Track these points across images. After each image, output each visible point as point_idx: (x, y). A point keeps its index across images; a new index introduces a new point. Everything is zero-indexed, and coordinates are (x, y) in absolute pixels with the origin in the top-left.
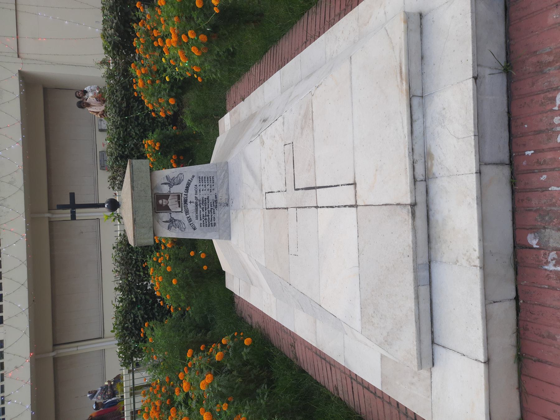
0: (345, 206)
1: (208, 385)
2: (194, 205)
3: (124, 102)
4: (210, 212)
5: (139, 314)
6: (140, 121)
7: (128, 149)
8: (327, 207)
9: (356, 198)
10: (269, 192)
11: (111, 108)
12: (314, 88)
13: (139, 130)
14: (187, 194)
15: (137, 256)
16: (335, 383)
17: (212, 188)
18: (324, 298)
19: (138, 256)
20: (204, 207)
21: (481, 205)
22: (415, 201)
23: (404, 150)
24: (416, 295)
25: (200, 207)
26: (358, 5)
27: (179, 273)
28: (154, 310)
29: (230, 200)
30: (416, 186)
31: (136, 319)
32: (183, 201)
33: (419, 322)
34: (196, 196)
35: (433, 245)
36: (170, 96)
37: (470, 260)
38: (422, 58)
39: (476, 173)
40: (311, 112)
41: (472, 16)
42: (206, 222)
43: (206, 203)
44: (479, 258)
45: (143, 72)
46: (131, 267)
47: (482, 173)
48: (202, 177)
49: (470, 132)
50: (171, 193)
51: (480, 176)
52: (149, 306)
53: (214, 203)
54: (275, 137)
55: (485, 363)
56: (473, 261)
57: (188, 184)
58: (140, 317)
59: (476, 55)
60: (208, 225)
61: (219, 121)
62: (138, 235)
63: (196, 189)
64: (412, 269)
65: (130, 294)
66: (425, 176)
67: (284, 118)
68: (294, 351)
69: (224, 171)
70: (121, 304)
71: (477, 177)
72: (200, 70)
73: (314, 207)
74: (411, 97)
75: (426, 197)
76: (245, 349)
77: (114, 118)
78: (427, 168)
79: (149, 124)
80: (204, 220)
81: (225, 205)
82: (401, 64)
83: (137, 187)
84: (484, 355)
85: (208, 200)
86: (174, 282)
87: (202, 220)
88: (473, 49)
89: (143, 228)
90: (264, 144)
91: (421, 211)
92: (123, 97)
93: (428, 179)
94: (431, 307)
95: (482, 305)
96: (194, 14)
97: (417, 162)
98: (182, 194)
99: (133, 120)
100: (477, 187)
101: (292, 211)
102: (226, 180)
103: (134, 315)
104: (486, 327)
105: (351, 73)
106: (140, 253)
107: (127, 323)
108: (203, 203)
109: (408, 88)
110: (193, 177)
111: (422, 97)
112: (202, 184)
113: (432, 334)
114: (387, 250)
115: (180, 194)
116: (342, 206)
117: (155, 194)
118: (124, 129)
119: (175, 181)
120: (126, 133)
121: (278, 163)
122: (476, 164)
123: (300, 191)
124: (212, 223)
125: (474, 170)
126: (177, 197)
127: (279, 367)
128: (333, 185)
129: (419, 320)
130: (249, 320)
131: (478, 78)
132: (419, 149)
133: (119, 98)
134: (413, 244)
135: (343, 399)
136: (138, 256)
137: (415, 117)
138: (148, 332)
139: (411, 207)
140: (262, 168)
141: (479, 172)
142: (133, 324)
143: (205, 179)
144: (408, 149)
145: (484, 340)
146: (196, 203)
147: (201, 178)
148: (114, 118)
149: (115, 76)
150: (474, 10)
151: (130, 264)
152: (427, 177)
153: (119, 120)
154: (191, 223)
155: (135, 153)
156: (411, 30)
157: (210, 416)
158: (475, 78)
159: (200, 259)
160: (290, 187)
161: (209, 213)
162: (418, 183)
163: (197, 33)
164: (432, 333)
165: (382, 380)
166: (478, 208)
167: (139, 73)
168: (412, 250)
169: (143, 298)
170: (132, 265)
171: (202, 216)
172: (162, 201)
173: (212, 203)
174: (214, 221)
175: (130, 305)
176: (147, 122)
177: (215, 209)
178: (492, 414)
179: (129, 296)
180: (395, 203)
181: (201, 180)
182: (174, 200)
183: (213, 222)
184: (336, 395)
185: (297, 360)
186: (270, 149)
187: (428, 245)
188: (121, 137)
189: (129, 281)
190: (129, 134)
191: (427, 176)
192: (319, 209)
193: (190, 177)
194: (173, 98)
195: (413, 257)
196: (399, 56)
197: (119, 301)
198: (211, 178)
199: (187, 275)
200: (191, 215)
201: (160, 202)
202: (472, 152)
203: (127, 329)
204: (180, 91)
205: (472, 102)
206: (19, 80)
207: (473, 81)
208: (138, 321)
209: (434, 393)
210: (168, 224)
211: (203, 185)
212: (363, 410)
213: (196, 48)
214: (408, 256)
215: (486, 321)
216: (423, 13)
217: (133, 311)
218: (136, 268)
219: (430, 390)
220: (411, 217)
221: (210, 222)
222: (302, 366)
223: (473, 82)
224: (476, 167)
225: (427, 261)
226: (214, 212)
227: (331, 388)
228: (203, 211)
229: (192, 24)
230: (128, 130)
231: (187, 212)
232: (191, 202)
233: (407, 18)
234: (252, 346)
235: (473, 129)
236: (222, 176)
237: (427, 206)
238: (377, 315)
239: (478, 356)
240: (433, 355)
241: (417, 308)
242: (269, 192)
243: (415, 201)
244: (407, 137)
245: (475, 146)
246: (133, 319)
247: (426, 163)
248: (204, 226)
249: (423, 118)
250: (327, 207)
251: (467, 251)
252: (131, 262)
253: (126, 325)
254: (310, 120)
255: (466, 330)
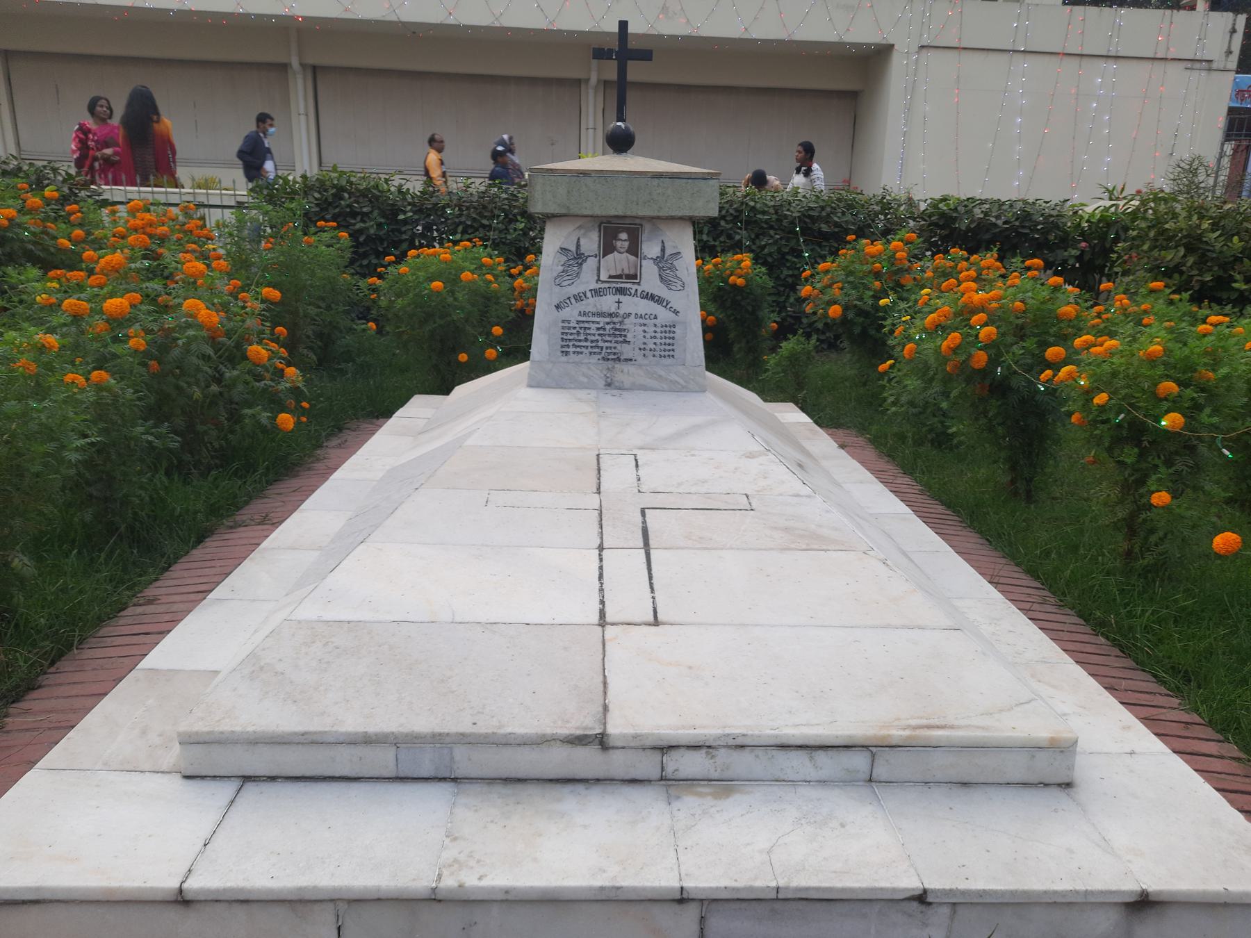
0: (602, 602)
1: (194, 316)
2: (613, 310)
3: (830, 227)
4: (594, 344)
5: (367, 225)
6: (789, 257)
7: (731, 229)
8: (601, 568)
9: (622, 624)
10: (636, 460)
11: (820, 201)
12: (882, 556)
13: (770, 254)
14: (639, 295)
15: (498, 229)
16: (164, 599)
17: (647, 353)
18: (381, 550)
19: (497, 232)
20: (607, 332)
21: (597, 901)
22: (613, 748)
23: (741, 724)
24: (374, 738)
25: (608, 323)
26: (1077, 662)
27: (455, 299)
28: (374, 257)
29: (620, 391)
30: (649, 752)
31: (359, 218)
32: (623, 285)
33: (302, 744)
34: (633, 316)
35: (499, 789)
36: (846, 308)
37: (456, 866)
38: (965, 784)
39: (682, 888)
40: (825, 547)
41: (1077, 892)
42: (572, 334)
43: (615, 337)
44: (460, 886)
45: (898, 255)
46: (474, 216)
47: (677, 907)
48: (674, 332)
49: (786, 879)
50: (643, 261)
51: (674, 900)
52: (384, 248)
53: (615, 354)
54: (765, 478)
55: (181, 891)
56: (452, 874)
57: (658, 300)
58: (362, 225)
59: (981, 900)
60: (565, 337)
61: (792, 405)
62: (553, 178)
63: (647, 317)
64: (442, 731)
65: (414, 209)
66: (673, 777)
67: (809, 496)
68: (253, 523)
69: (685, 382)
70: (393, 189)
71: (672, 889)
72: (907, 356)
73: (602, 543)
74: (870, 748)
75: (621, 778)
76: (269, 414)
77: (798, 205)
78: (693, 785)
79: (782, 276)
80: (578, 329)
81: (609, 380)
82: (952, 727)
83: (659, 186)
84: (202, 891)
85: (621, 342)
86: (437, 284)
87: (577, 325)
88: (995, 892)
89: (569, 192)
90: (748, 457)
91: (587, 761)
92: (843, 227)
93: (664, 785)
94: (339, 778)
95: (335, 890)
96: (1030, 343)
97: (710, 756)
98: (639, 284)
99: (793, 243)
100: (644, 889)
101: (594, 501)
102: (665, 386)
103: (367, 214)
104: (275, 898)
105: (920, 628)
106: (503, 236)
107: (350, 198)
108: (616, 330)
109: (894, 743)
110: (676, 312)
111: (870, 780)
112: (658, 330)
113: (269, 777)
114: (492, 680)
115: (638, 281)
116: (603, 597)
117: (641, 225)
118: (772, 223)
119: (668, 272)
120: (765, 226)
121: (704, 482)
122: (704, 889)
123: (640, 519)
124: (568, 346)
125: (688, 884)
126: (632, 272)
127: (217, 487)
128: (654, 581)
129: (308, 743)
130: (335, 442)
131: (923, 908)
132: (742, 763)
133: (839, 217)
134: (505, 735)
135: (122, 613)
136: (497, 232)
137: (821, 756)
138: (326, 236)
139: (599, 734)
140: (693, 452)
141: (682, 899)
142: (348, 210)
143: (670, 338)
144: (744, 735)
145: (241, 890)
146: (617, 315)
147: (672, 329)
148: (798, 205)
149: (886, 216)
150: (1093, 900)
151: (480, 214)
152: (670, 783)
153: (794, 215)
154: (573, 300)
155: (721, 242)
156: (1033, 757)
157: (120, 313)
158: (922, 898)
159: (483, 348)
160: (648, 501)
161: (592, 341)
162: (656, 756)
163: (991, 346)
164: (273, 779)
165: (161, 670)
166: (590, 889)
167: (896, 246)
168: (490, 731)
169: (404, 237)
170: (477, 217)
171: (587, 325)
172: (625, 240)
173: (613, 351)
174: (574, 352)
175: (389, 208)
176: (786, 272)
177: (600, 357)
178: (35, 910)
179: (410, 207)
180: (609, 702)
181: (668, 329)
182: (625, 265)
183: (571, 349)
184: (135, 600)
185: (231, 527)
186: (736, 469)
187: (499, 777)
188: (758, 216)
189: (444, 208)
190: (764, 234)
191: (674, 782)
192: (597, 552)
193: (675, 304)
194: (842, 315)
195: (470, 735)
196: (970, 725)
197: (401, 186)
198: (671, 353)
199: (450, 315)
200: (591, 300)
201: (624, 236)
202: (736, 881)
203: (338, 196)
204: (857, 330)
205: (864, 885)
206: (875, 45)
207: (917, 889)
208: (353, 221)
209: (113, 776)
210: (573, 249)
211: (655, 332)
212: (88, 653)
213: (958, 341)
214: (474, 724)
215: (290, 901)
216: (1074, 789)
217: (376, 213)
218: (471, 226)
219: (122, 768)
220: (572, 732)
221: (571, 344)
222: (215, 537)
223: (913, 889)
224: (696, 888)
225: (459, 773)
226: (594, 353)
227: (150, 592)
228: (598, 329)
229: (1010, 339)
230: (772, 232)
231: (597, 293)
232: (619, 302)
233: (1063, 748)
234: (271, 431)
235: (794, 884)
236: (673, 377)
237: (598, 780)
238: (330, 652)
239: (201, 875)
240: (215, 777)
241: (341, 740)
242: (636, 460)
243: (613, 748)
244: (772, 732)
245: (751, 889)
246: (358, 210)
247: (706, 783)
248: (563, 328)
249: (818, 779)
250: (601, 568)
251: (478, 861)
252: (486, 217)
253: (346, 195)
254: (808, 545)
255: (272, 853)
